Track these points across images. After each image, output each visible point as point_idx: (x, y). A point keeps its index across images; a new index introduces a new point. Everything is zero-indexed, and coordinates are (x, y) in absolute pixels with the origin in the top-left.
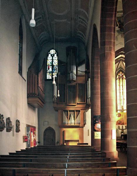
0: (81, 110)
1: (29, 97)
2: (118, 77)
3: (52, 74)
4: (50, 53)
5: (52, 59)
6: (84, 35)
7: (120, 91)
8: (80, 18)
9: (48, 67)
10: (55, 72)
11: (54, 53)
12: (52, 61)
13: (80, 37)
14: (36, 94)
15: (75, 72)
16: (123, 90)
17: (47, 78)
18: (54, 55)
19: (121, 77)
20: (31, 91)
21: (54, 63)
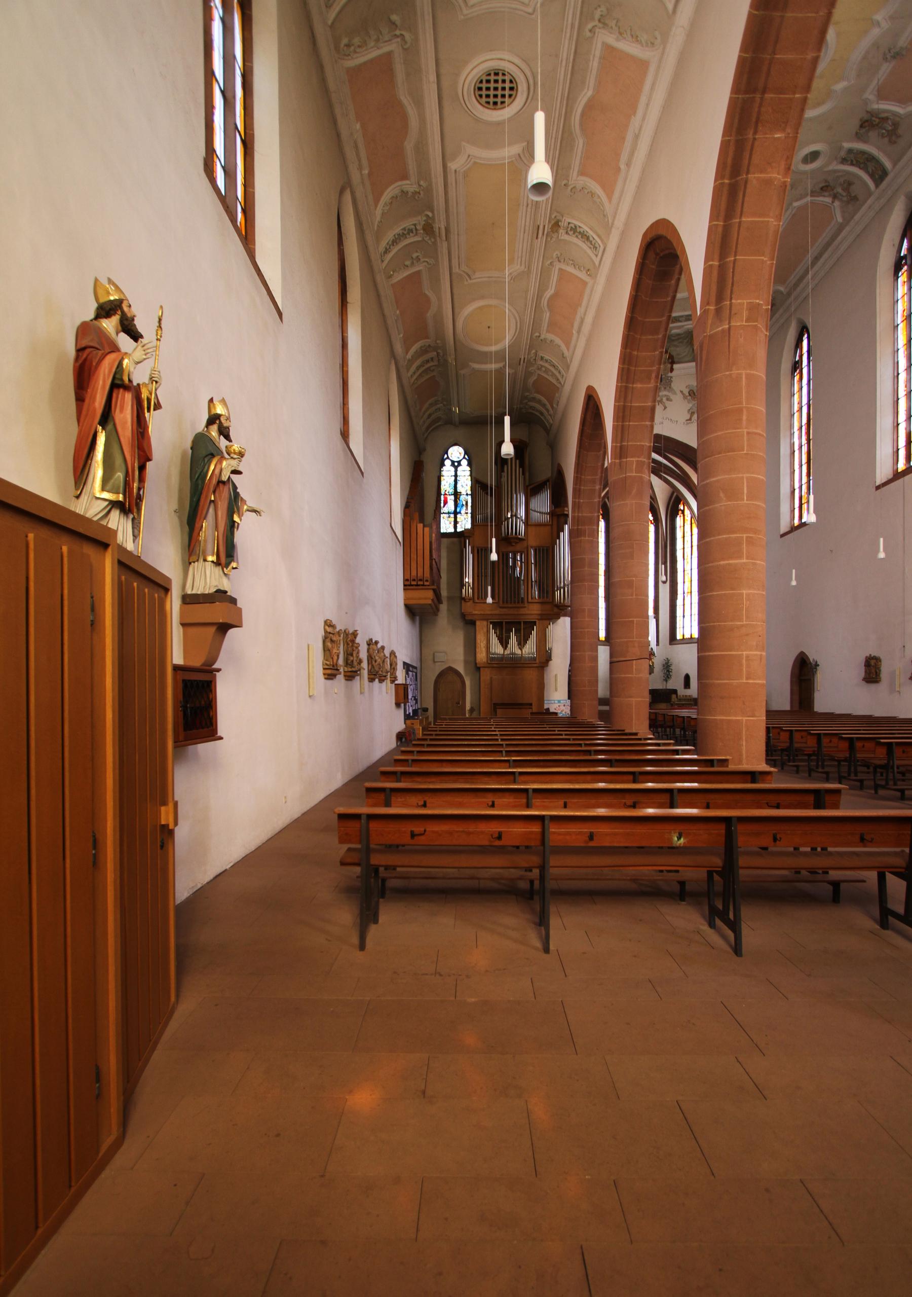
0: (538, 619)
3: (455, 518)
5: (456, 476)
6: (549, 406)
8: (542, 358)
9: (442, 497)
10: (463, 511)
11: (459, 455)
12: (456, 481)
13: (537, 411)
14: (427, 581)
15: (522, 513)
17: (442, 531)
18: (459, 463)
20: (414, 573)
21: (459, 486)
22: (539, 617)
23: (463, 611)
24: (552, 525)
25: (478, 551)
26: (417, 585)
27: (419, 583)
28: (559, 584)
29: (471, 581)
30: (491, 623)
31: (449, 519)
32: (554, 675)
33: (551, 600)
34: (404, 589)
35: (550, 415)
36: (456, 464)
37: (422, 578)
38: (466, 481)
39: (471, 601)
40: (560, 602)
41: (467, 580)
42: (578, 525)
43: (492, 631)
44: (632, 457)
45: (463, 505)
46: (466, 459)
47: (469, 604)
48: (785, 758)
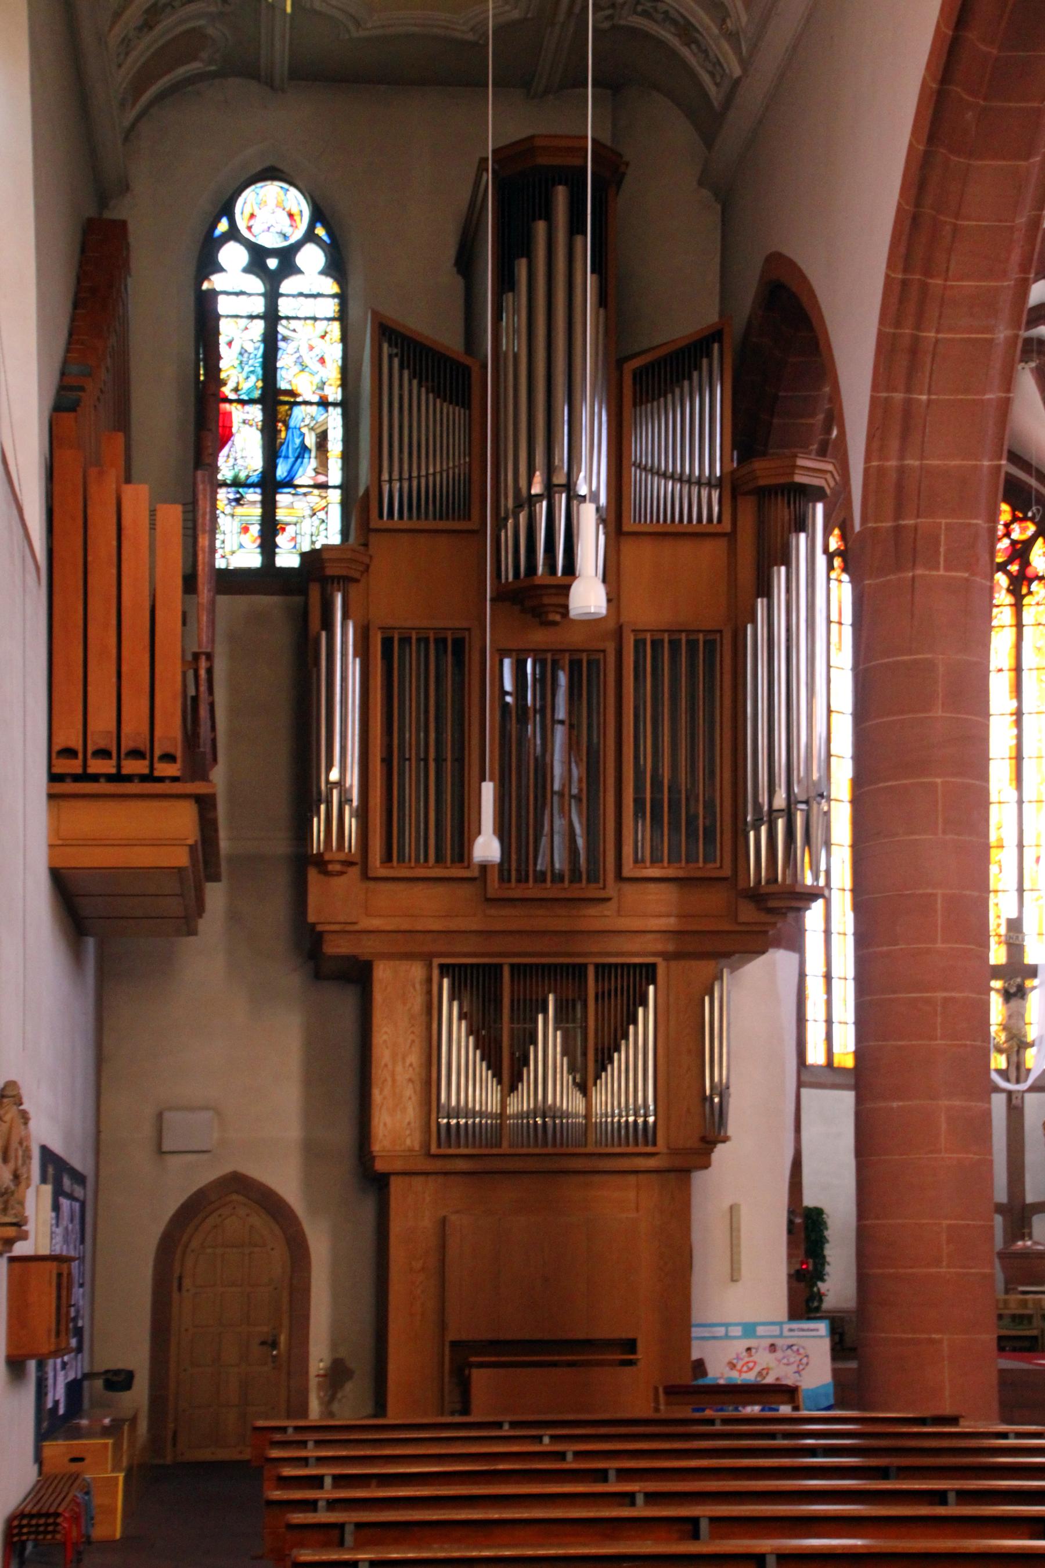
0: (667, 956)
1: (69, 787)
3: (269, 507)
4: (241, 224)
5: (271, 317)
10: (306, 475)
12: (271, 343)
14: (169, 758)
16: (1019, 724)
18: (287, 256)
20: (102, 722)
21: (285, 360)
22: (671, 947)
23: (312, 918)
25: (387, 643)
26: (118, 778)
27: (131, 766)
28: (764, 799)
29: (353, 780)
30: (445, 970)
31: (239, 510)
32: (726, 1206)
33: (727, 872)
34: (51, 796)
35: (733, 38)
36: (272, 263)
37: (143, 745)
38: (317, 342)
39: (354, 872)
40: (773, 879)
41: (334, 775)
42: (898, 514)
43: (449, 1010)
45: (304, 449)
47: (339, 883)
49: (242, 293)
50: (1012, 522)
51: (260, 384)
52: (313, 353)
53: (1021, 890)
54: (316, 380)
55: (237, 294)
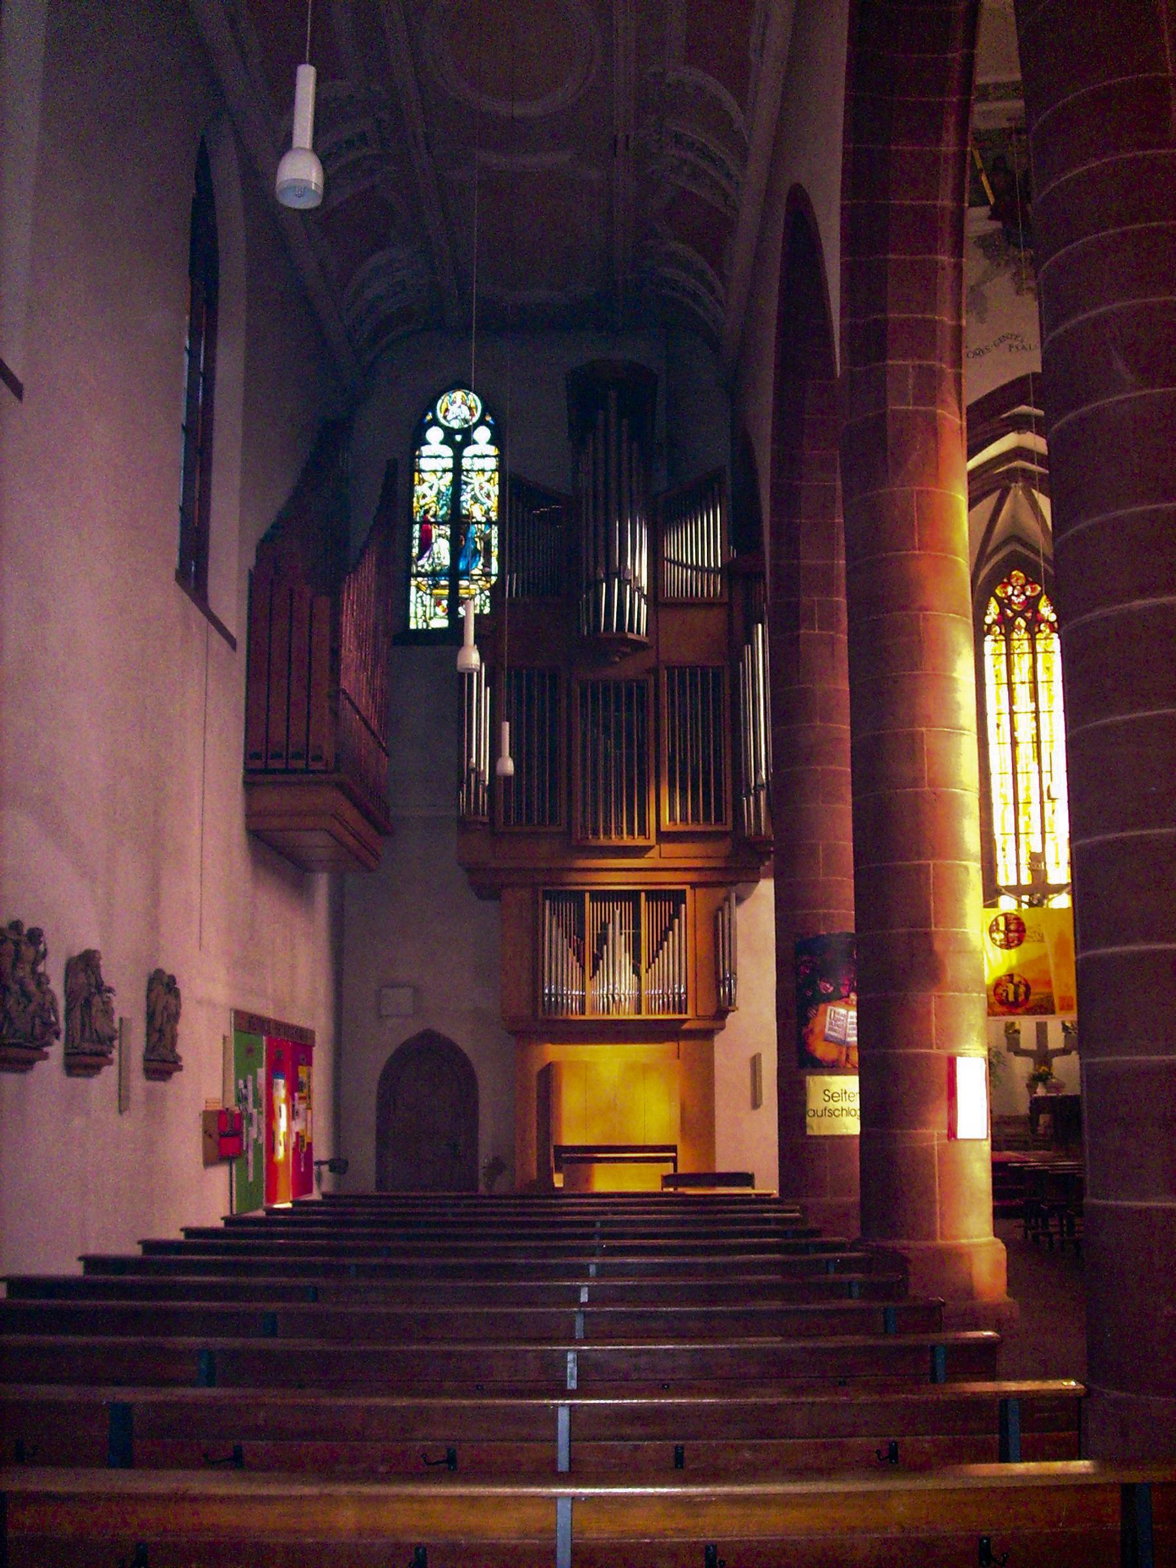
0: (693, 885)
2: (993, 609)
3: (454, 588)
4: (440, 415)
5: (457, 470)
7: (1013, 730)
11: (465, 413)
16: (1037, 719)
19: (1020, 614)
21: (465, 497)
24: (729, 606)
31: (435, 591)
44: (904, 357)
46: (488, 425)
48: (262, 1414)
49: (439, 456)
50: (1026, 584)
51: (449, 512)
52: (482, 492)
53: (1043, 833)
54: (485, 508)
55: (436, 457)
